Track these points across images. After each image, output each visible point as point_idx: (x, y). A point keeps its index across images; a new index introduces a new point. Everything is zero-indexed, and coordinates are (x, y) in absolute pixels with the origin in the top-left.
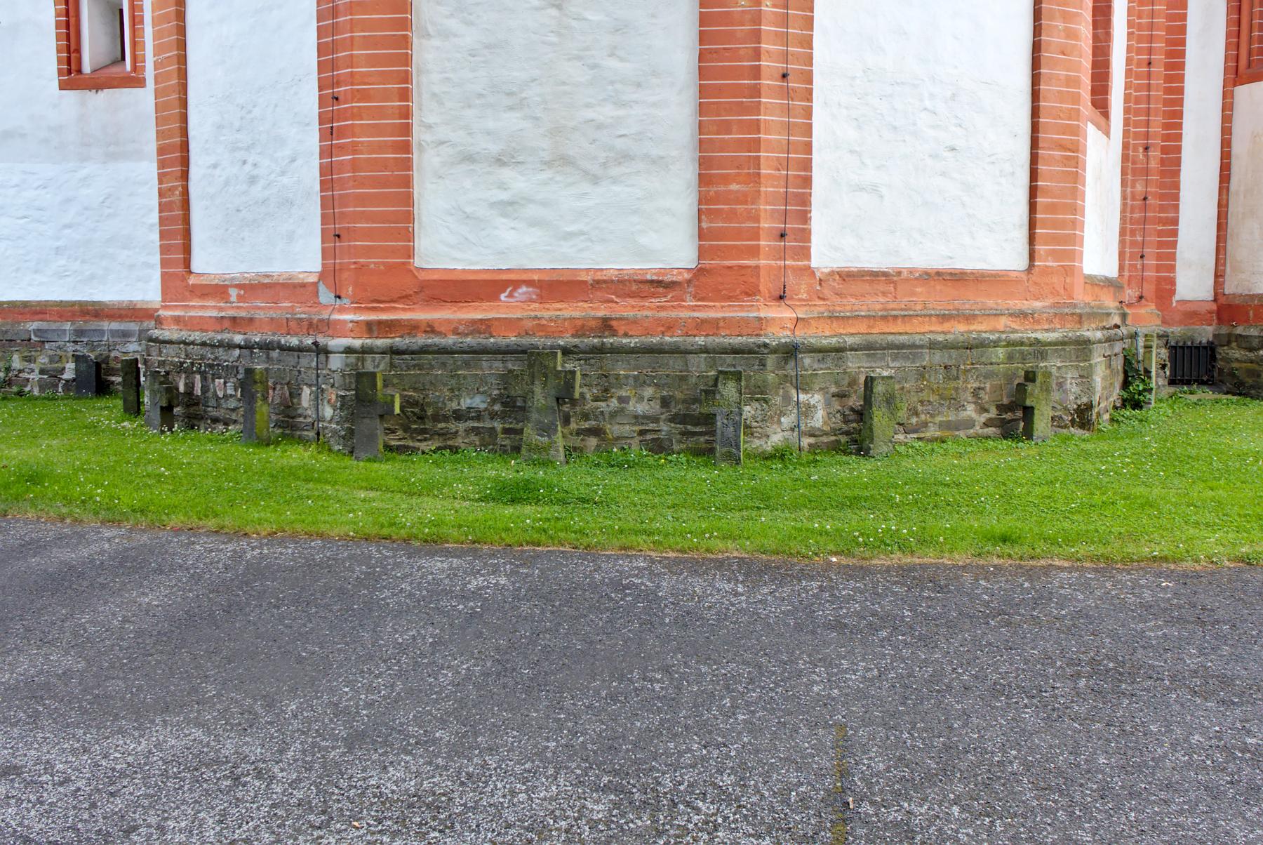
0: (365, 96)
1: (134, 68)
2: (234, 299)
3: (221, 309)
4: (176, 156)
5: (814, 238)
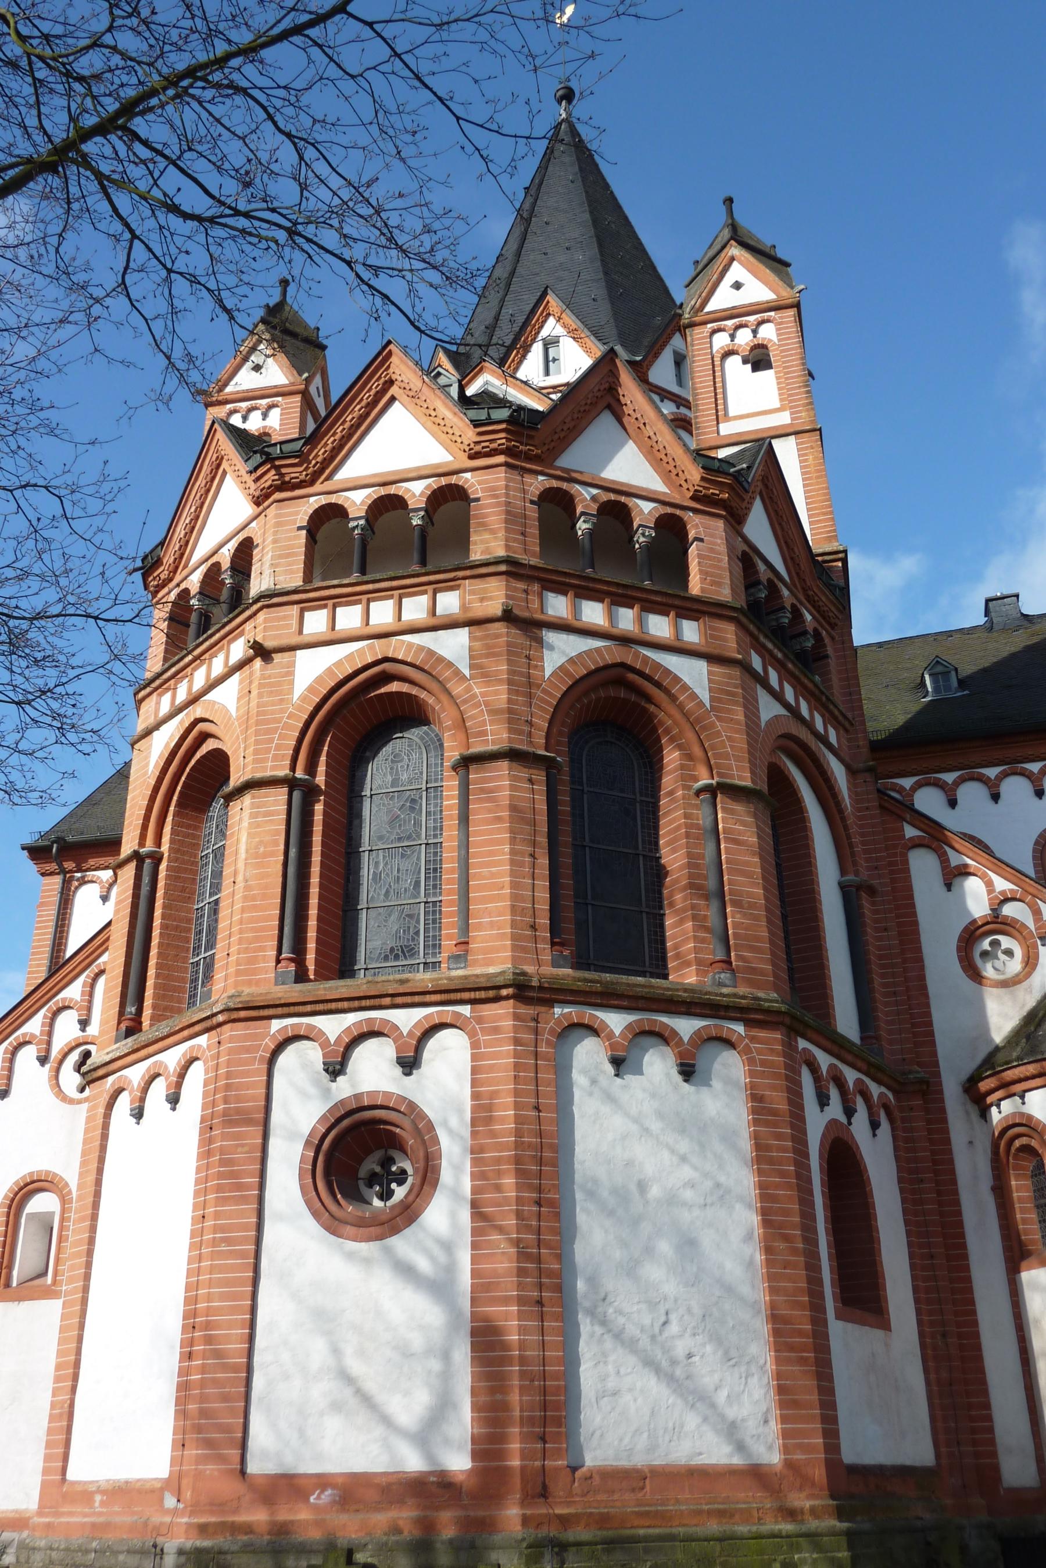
0: (227, 1283)
1: (55, 1282)
2: (97, 1504)
3: (85, 1515)
4: (70, 1372)
5: (936, 1035)
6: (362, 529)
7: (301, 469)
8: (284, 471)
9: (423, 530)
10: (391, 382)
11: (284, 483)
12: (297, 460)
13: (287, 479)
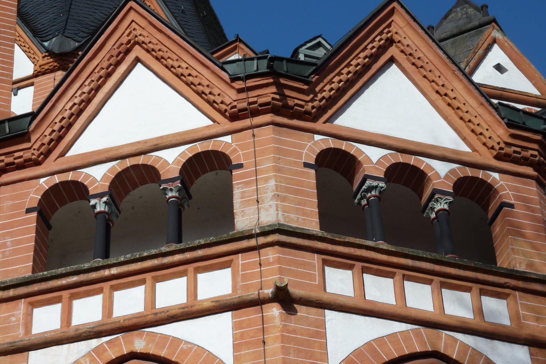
6: (380, 192)
7: (308, 98)
8: (287, 92)
9: (179, 206)
10: (390, 42)
11: (286, 106)
12: (306, 87)
13: (291, 103)
